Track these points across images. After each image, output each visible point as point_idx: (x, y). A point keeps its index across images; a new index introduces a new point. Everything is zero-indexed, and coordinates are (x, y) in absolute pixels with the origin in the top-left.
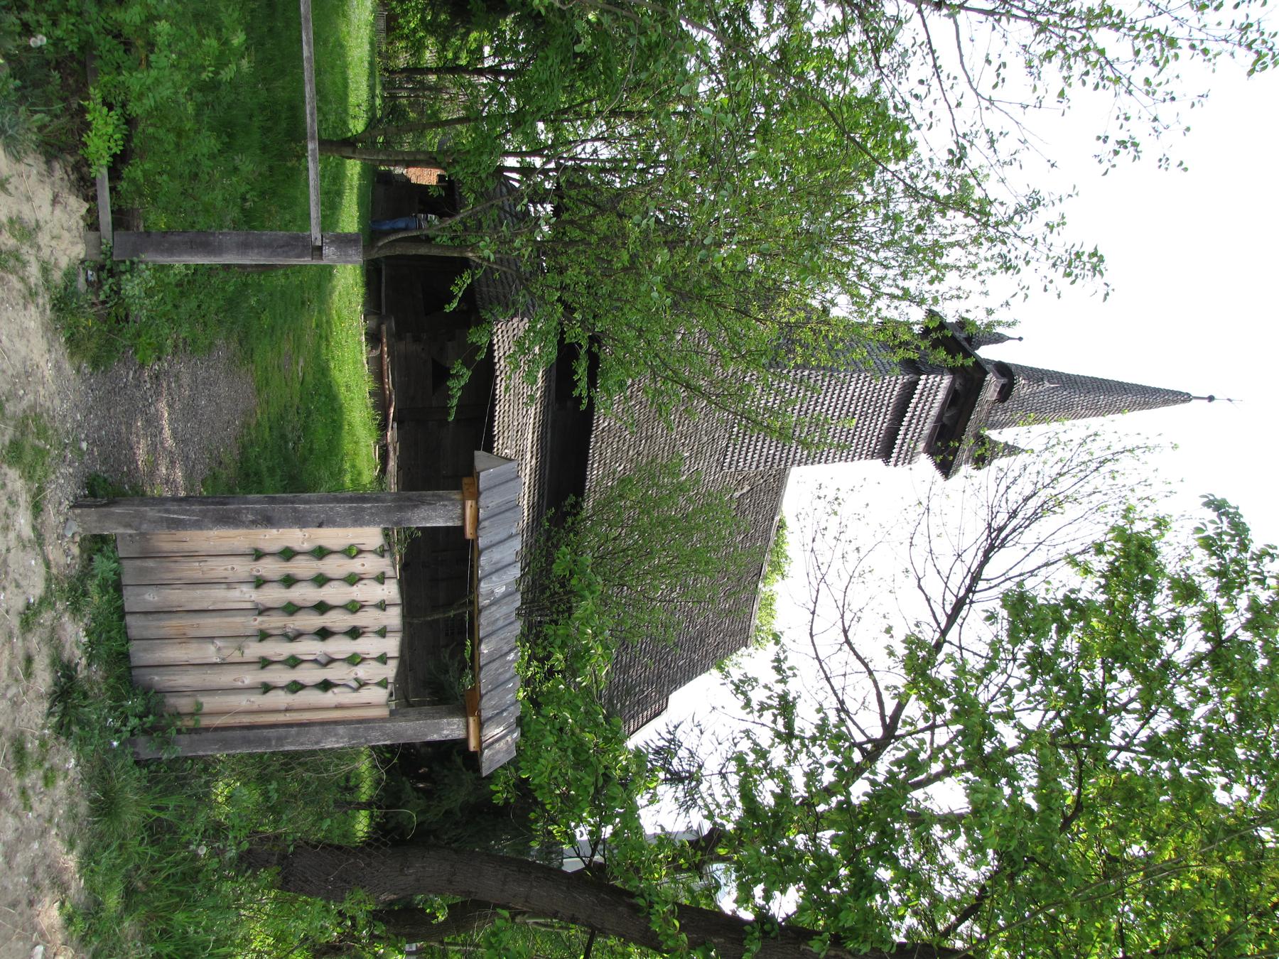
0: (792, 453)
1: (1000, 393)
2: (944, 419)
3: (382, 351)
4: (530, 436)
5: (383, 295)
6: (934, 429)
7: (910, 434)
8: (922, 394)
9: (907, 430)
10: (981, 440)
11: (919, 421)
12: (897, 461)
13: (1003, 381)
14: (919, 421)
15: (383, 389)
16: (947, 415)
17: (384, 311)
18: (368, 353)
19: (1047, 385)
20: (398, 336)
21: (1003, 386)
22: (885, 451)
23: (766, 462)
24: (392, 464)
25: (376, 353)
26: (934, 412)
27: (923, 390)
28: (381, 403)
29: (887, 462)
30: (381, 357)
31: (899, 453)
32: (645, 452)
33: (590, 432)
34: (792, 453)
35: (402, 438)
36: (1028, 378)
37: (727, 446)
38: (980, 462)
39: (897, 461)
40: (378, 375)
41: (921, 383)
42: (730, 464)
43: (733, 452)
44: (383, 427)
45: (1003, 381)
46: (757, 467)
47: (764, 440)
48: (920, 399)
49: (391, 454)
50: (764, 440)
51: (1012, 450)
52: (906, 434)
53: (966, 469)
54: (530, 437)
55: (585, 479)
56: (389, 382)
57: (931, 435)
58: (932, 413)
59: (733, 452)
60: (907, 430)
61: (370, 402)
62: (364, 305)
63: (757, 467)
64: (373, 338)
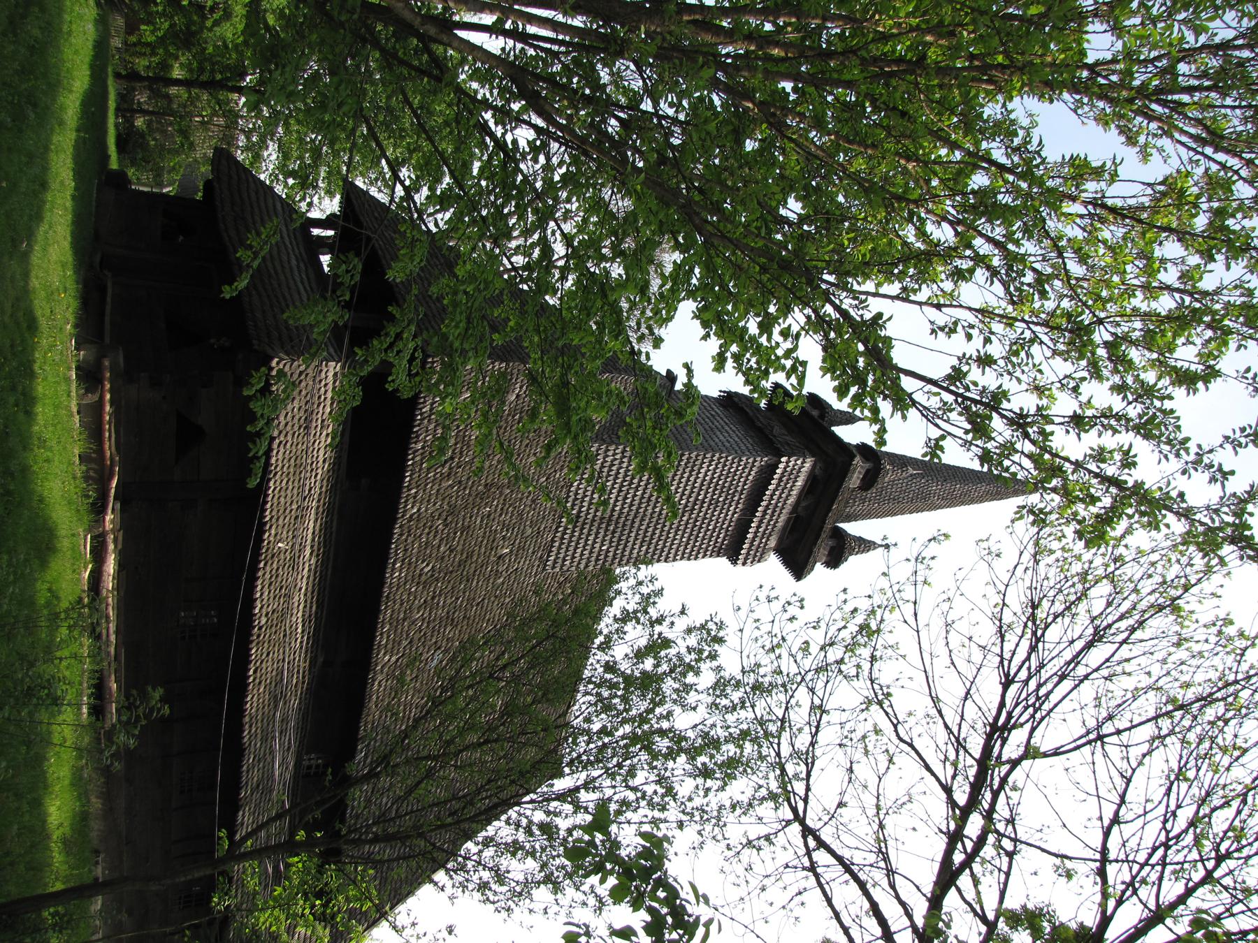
0: (628, 549)
1: (863, 480)
2: (800, 509)
3: (102, 397)
4: (311, 525)
5: (107, 319)
6: (789, 520)
7: (764, 526)
8: (780, 480)
9: (761, 522)
10: (840, 535)
11: (774, 511)
12: (746, 559)
13: (867, 465)
14: (774, 511)
15: (101, 451)
16: (803, 504)
17: (107, 340)
18: (80, 397)
19: (911, 471)
20: (124, 378)
21: (868, 471)
22: (733, 551)
23: (597, 560)
24: (111, 566)
25: (92, 398)
26: (791, 501)
27: (783, 475)
28: (93, 460)
29: (734, 562)
30: (100, 404)
31: (750, 549)
32: (459, 548)
33: (395, 520)
34: (628, 549)
35: (126, 525)
36: (892, 464)
37: (553, 541)
38: (834, 561)
39: (746, 559)
40: (94, 431)
41: (782, 466)
42: (555, 562)
43: (560, 548)
44: (98, 509)
45: (867, 465)
46: (587, 566)
47: (597, 533)
48: (778, 485)
49: (111, 547)
50: (597, 533)
51: (865, 545)
52: (759, 527)
53: (819, 568)
54: (311, 525)
55: (383, 583)
56: (109, 448)
57: (784, 528)
58: (789, 502)
59: (560, 548)
60: (761, 522)
61: (79, 470)
62: (76, 326)
63: (587, 566)
64: (89, 377)
